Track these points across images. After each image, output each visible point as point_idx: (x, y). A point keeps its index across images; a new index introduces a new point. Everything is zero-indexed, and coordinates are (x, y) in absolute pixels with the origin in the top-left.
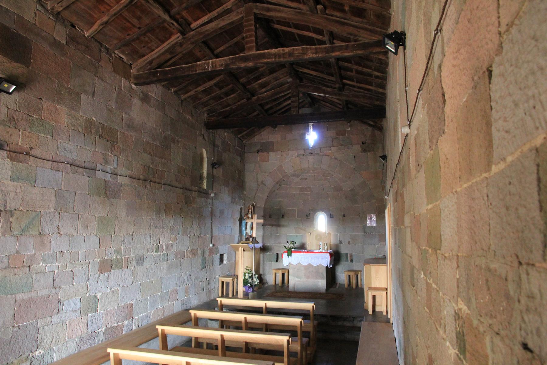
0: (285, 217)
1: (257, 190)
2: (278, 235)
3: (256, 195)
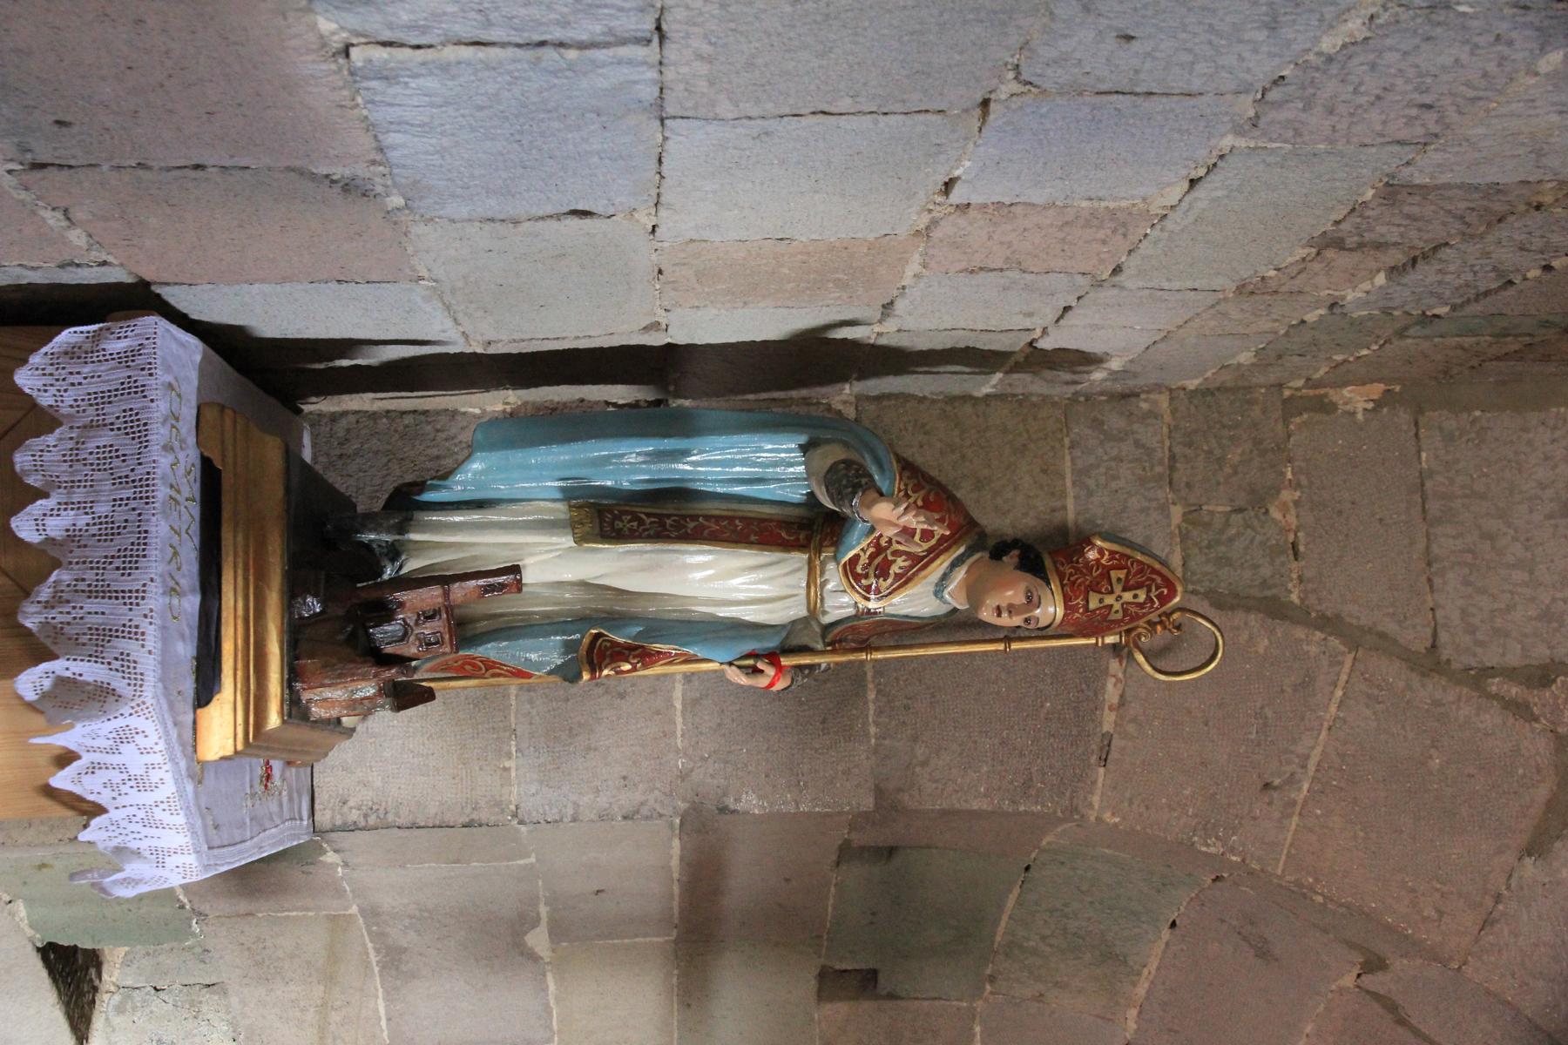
0: (839, 1010)
1: (1430, 662)
2: (538, 940)
3: (1313, 643)
